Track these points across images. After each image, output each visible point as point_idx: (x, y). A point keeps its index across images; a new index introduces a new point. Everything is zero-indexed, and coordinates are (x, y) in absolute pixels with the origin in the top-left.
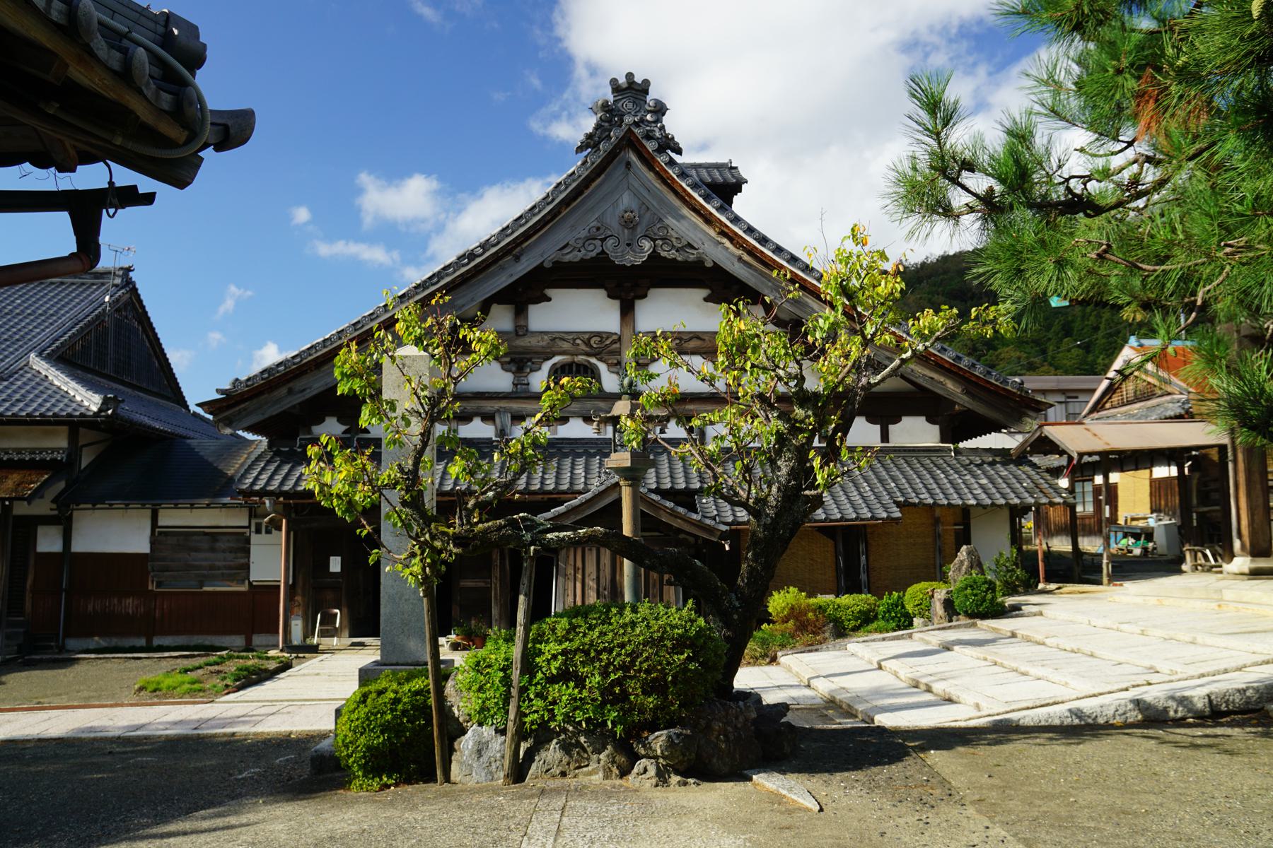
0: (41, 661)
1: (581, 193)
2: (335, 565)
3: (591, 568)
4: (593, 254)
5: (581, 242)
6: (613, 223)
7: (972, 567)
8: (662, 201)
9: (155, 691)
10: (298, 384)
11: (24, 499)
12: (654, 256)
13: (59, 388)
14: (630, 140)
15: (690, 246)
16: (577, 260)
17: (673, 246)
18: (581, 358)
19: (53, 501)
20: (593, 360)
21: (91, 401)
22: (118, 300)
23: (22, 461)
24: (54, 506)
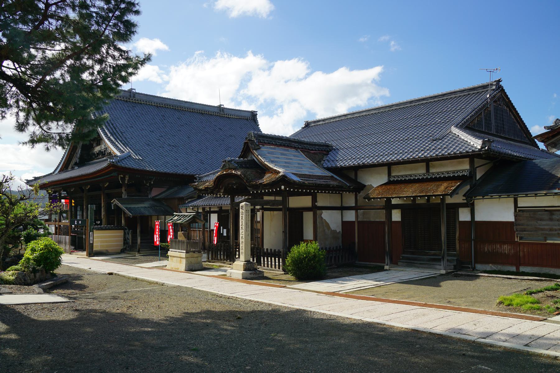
0: (462, 275)
9: (509, 305)
11: (448, 195)
13: (464, 140)
19: (464, 196)
21: (476, 143)
22: (494, 96)
23: (449, 177)
24: (465, 198)
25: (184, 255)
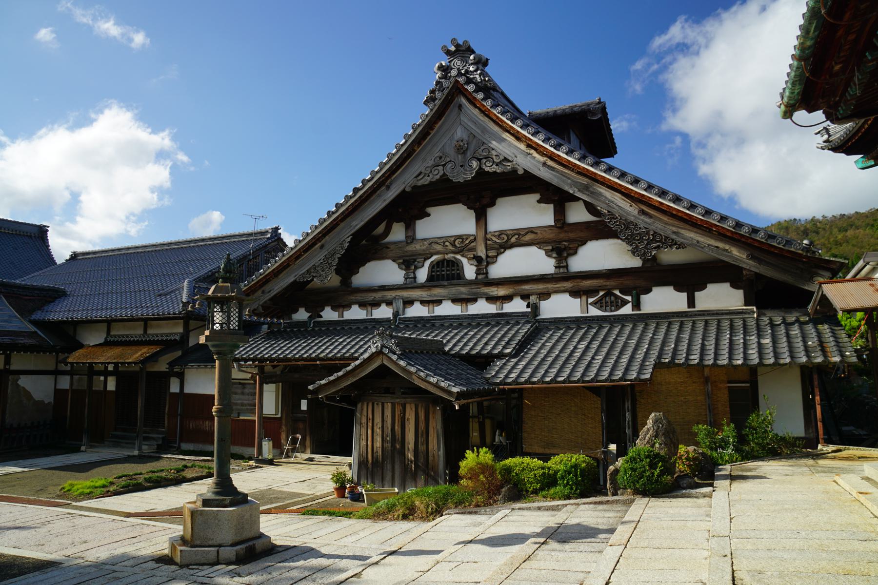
1: (428, 134)
2: (304, 405)
3: (378, 420)
4: (438, 177)
5: (429, 169)
6: (451, 151)
7: (656, 436)
8: (484, 130)
10: (267, 288)
12: (481, 172)
14: (458, 88)
15: (506, 160)
16: (427, 183)
17: (494, 162)
18: (449, 256)
20: (459, 257)
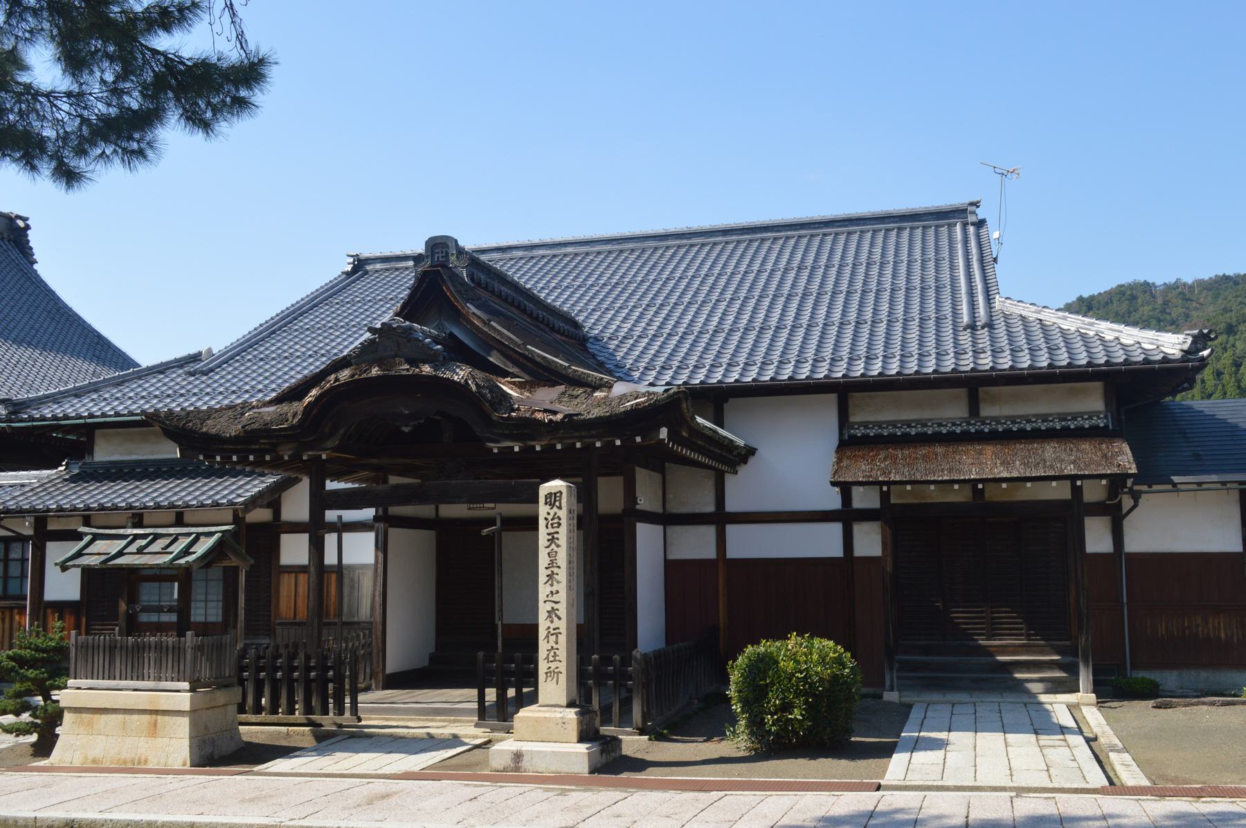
25: (183, 700)
